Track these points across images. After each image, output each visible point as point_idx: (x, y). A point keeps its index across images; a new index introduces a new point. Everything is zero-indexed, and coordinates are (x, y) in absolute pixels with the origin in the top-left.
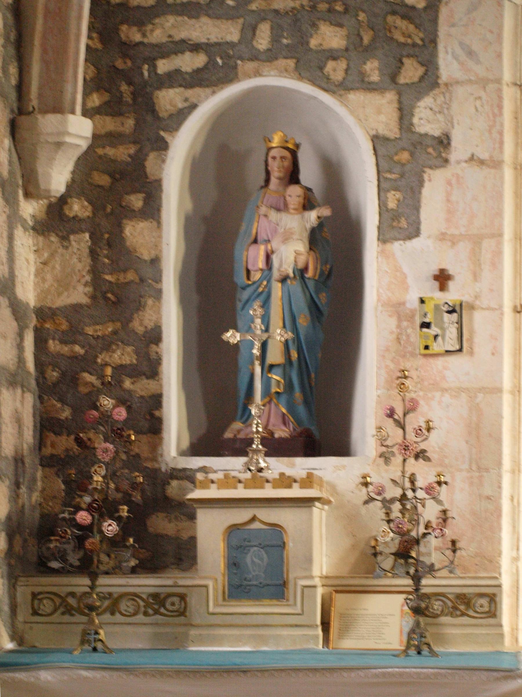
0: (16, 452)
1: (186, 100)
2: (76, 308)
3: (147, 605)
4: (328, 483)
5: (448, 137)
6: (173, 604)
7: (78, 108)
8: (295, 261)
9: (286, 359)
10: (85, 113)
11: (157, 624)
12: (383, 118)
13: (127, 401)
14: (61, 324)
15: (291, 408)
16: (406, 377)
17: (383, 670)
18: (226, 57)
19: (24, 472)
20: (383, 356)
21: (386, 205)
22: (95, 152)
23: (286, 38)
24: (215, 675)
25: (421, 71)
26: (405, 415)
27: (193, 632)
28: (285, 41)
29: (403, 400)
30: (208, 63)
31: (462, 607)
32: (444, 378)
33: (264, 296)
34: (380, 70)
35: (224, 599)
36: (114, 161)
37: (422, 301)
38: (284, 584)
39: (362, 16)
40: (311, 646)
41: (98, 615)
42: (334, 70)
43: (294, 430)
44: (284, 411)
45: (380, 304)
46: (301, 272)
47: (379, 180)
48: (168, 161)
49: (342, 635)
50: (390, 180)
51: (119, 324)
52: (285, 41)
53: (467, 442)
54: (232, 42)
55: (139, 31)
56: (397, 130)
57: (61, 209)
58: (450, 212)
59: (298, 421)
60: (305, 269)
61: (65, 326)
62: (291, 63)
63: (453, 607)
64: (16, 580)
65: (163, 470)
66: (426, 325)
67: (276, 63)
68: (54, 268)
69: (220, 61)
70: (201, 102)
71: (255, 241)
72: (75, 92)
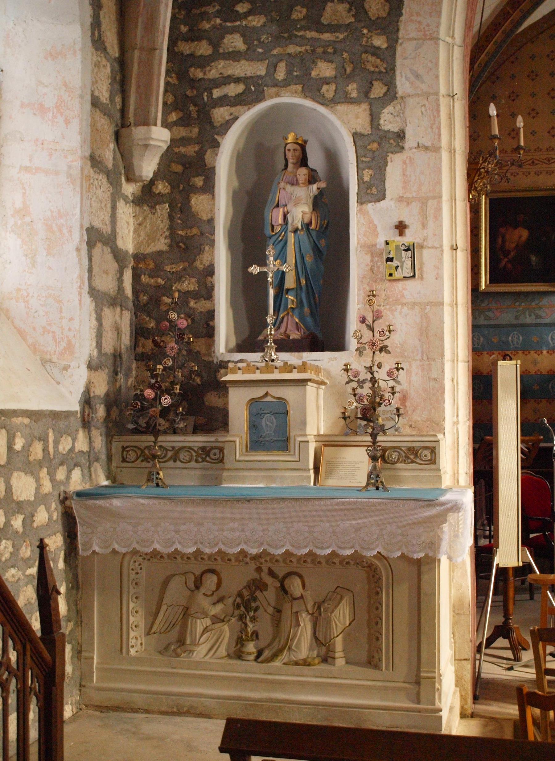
0: (115, 350)
1: (231, 114)
2: (160, 253)
3: (198, 455)
4: (324, 370)
5: (403, 132)
6: (215, 454)
7: (159, 122)
8: (303, 218)
9: (297, 285)
10: (165, 124)
11: (205, 469)
12: (360, 121)
13: (192, 315)
14: (149, 265)
15: (302, 318)
16: (374, 296)
17: (343, 500)
18: (257, 85)
19: (121, 364)
20: (362, 282)
21: (363, 179)
22: (173, 150)
23: (296, 72)
24: (228, 503)
25: (384, 89)
26: (373, 322)
27: (225, 474)
28: (295, 74)
29: (373, 311)
30: (245, 90)
31: (412, 457)
32: (403, 295)
33: (282, 243)
34: (357, 90)
35: (247, 451)
36: (185, 156)
37: (387, 243)
38: (287, 440)
39: (345, 55)
40: (305, 484)
41: (159, 462)
42: (328, 91)
43: (304, 333)
44: (297, 320)
45: (359, 246)
46: (307, 226)
47: (357, 162)
48: (219, 154)
49: (327, 477)
50: (365, 162)
51: (187, 264)
52: (295, 74)
53: (420, 340)
54: (260, 76)
55: (202, 71)
56: (369, 129)
57: (151, 188)
58: (406, 183)
59: (307, 327)
60: (310, 223)
61: (152, 266)
62: (299, 88)
63: (405, 457)
64: (112, 438)
65: (215, 362)
66: (390, 260)
67: (289, 87)
68: (146, 227)
69: (253, 88)
70: (241, 115)
71: (278, 206)
72: (157, 112)
